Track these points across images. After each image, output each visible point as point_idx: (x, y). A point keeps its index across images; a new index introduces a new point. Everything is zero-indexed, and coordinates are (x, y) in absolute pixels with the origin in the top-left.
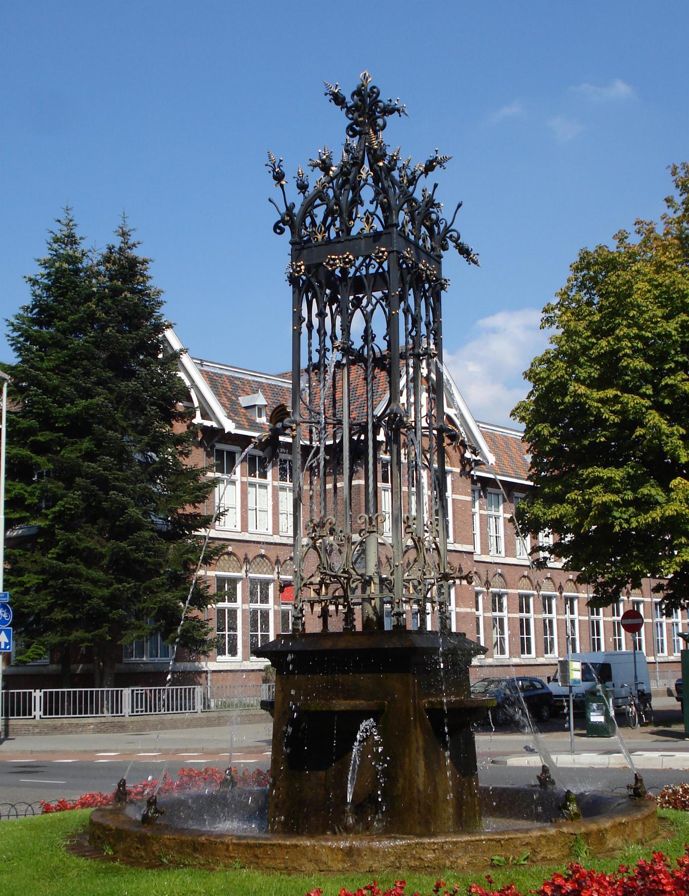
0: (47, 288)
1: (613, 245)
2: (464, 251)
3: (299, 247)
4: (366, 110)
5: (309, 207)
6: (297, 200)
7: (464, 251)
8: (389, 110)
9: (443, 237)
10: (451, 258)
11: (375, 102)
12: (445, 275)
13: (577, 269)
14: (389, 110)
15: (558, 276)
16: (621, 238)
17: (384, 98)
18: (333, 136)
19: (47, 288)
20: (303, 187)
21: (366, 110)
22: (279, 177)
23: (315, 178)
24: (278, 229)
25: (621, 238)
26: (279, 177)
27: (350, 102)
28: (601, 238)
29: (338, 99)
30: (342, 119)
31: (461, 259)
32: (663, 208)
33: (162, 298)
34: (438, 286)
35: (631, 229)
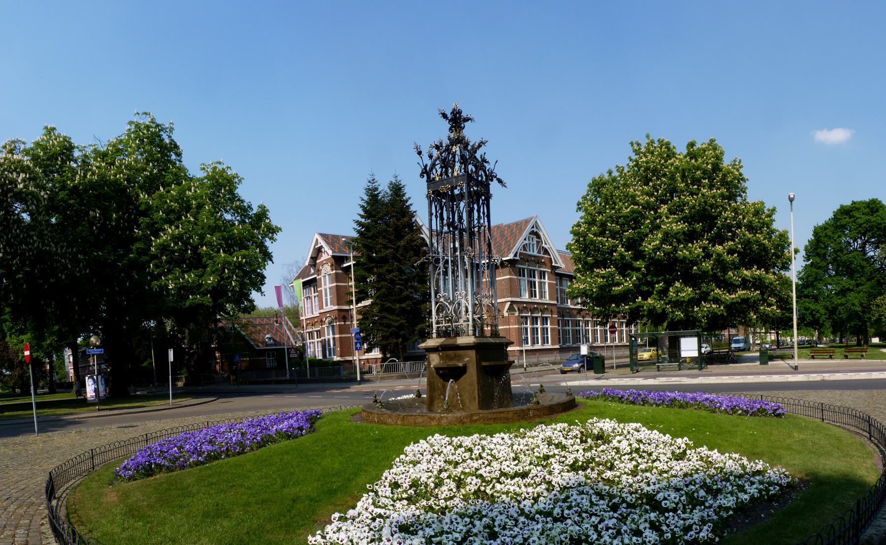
0: (366, 202)
1: (606, 177)
2: (500, 181)
3: (430, 181)
4: (457, 120)
5: (433, 165)
6: (429, 162)
7: (500, 181)
8: (467, 120)
9: (490, 176)
10: (494, 186)
11: (460, 116)
12: (491, 192)
13: (646, 173)
14: (467, 120)
15: (583, 189)
16: (610, 173)
17: (464, 115)
18: (443, 132)
19: (366, 202)
20: (431, 157)
21: (457, 120)
22: (420, 153)
23: (435, 153)
24: (422, 175)
25: (610, 173)
26: (420, 153)
27: (449, 116)
28: (600, 169)
29: (444, 116)
30: (447, 125)
31: (499, 185)
32: (628, 161)
33: (384, 188)
34: (488, 197)
35: (614, 170)
